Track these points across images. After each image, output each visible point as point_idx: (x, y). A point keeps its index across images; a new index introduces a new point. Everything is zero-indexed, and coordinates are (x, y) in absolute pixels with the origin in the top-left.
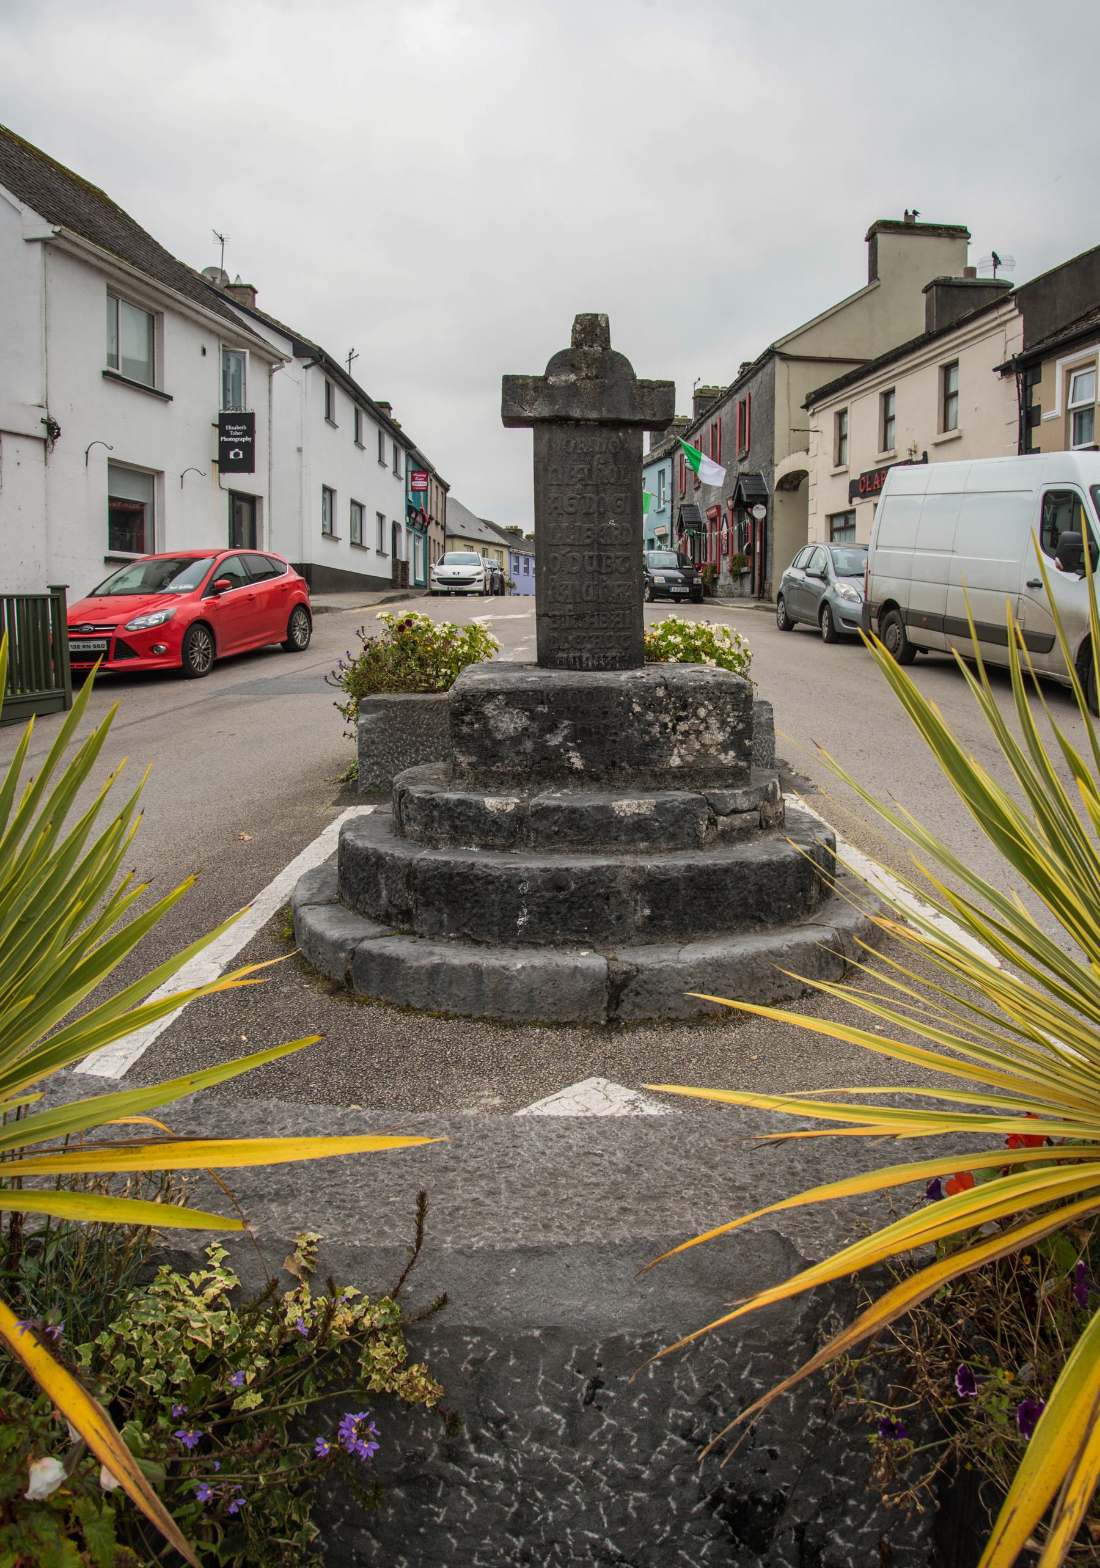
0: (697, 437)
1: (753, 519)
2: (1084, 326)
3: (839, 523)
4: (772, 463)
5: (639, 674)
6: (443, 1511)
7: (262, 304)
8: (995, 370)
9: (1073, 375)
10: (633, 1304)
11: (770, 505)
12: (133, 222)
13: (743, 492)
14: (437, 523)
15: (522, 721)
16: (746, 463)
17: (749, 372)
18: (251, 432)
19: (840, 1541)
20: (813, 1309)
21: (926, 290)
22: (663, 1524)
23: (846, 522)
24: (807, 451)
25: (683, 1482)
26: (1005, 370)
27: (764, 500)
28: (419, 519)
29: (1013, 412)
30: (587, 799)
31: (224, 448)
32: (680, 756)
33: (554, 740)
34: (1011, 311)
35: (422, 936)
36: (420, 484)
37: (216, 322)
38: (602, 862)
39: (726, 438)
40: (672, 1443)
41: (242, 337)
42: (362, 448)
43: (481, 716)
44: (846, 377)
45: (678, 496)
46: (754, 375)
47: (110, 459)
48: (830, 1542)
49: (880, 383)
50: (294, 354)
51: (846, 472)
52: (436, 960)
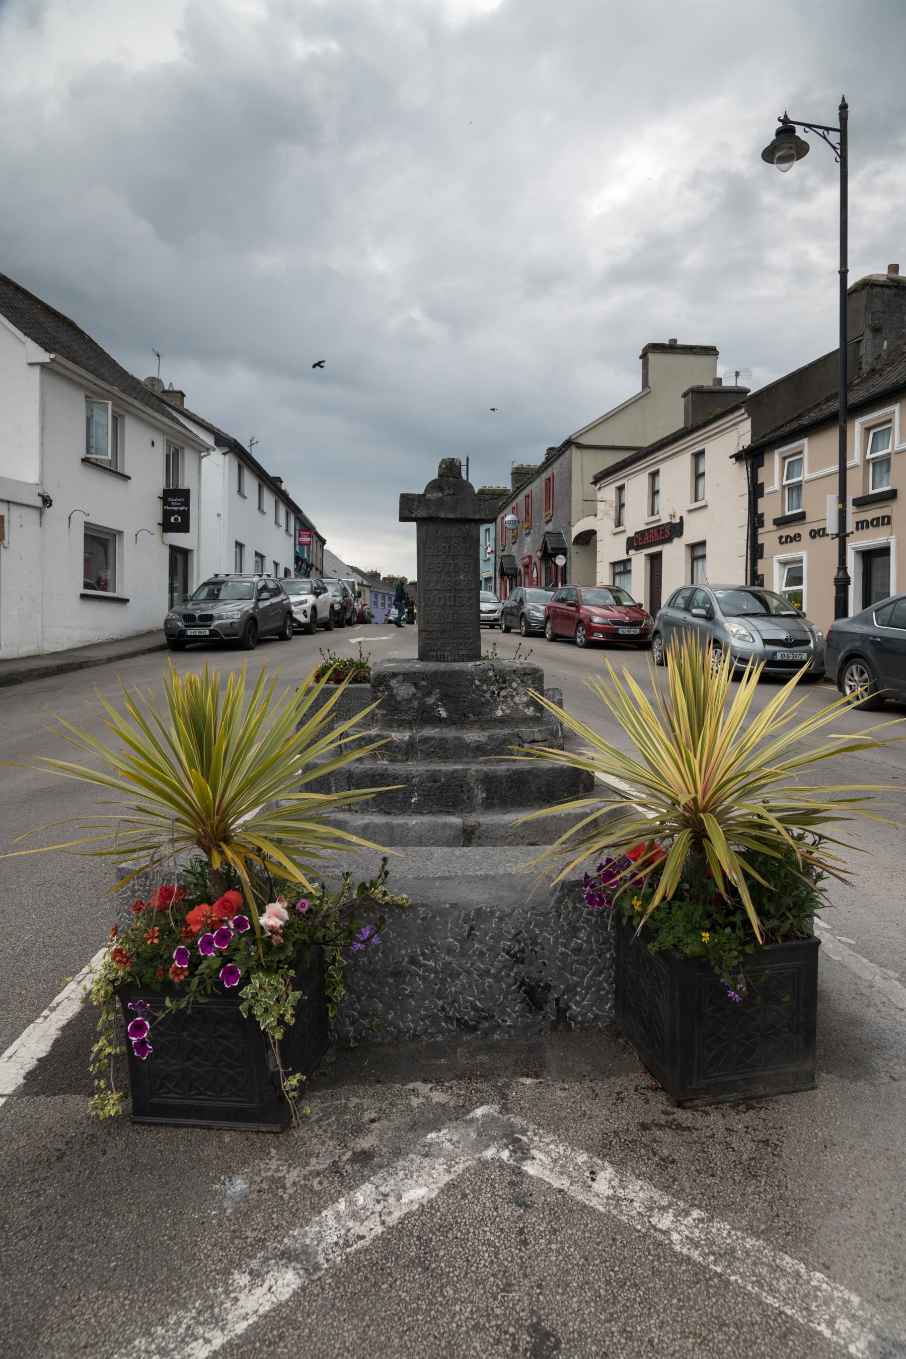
0: (514, 504)
1: (556, 565)
2: (795, 425)
3: (620, 569)
4: (570, 525)
5: (478, 663)
6: (409, 988)
7: (188, 405)
8: (731, 457)
9: (787, 461)
10: (487, 896)
11: (568, 556)
12: (96, 344)
13: (549, 546)
14: (317, 569)
15: (413, 690)
16: (550, 524)
17: (554, 455)
18: (187, 503)
19: (574, 1007)
20: (559, 898)
21: (684, 396)
22: (499, 994)
23: (625, 568)
24: (596, 515)
25: (508, 975)
26: (738, 457)
27: (564, 551)
28: (304, 566)
29: (743, 486)
30: (450, 733)
31: (166, 515)
32: (502, 710)
33: (431, 701)
34: (742, 414)
35: (356, 812)
36: (306, 539)
37: (162, 423)
38: (458, 767)
39: (536, 506)
40: (503, 956)
41: (181, 433)
42: (264, 513)
43: (389, 688)
44: (624, 461)
45: (500, 548)
46: (557, 459)
47: (85, 523)
48: (570, 1008)
49: (649, 466)
50: (216, 444)
51: (624, 531)
52: (367, 821)
